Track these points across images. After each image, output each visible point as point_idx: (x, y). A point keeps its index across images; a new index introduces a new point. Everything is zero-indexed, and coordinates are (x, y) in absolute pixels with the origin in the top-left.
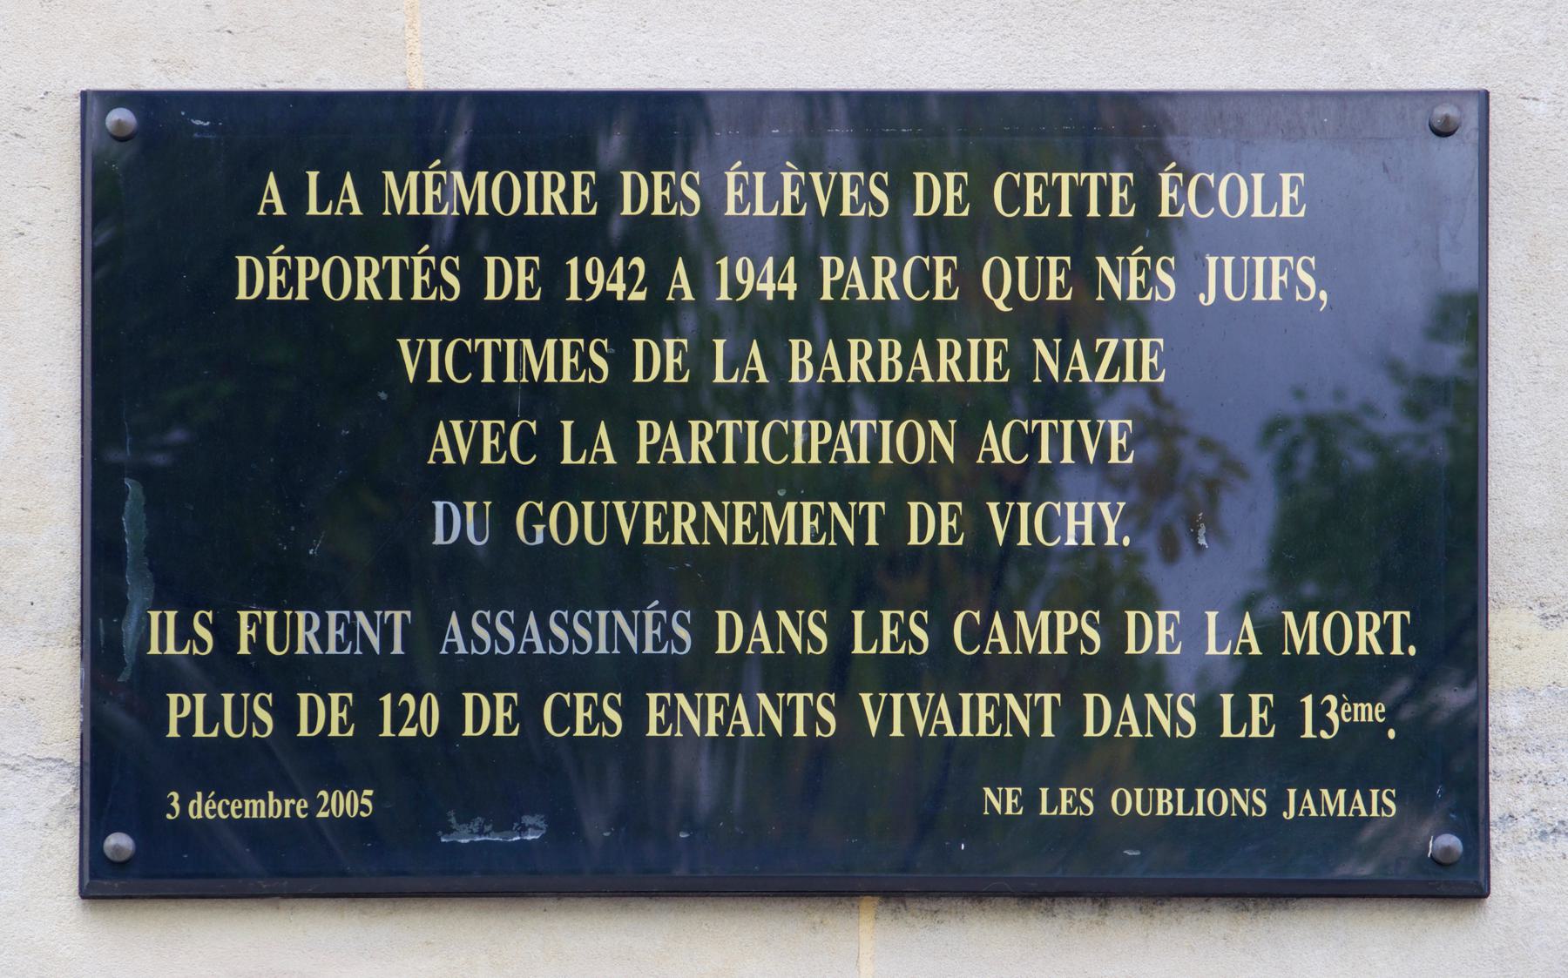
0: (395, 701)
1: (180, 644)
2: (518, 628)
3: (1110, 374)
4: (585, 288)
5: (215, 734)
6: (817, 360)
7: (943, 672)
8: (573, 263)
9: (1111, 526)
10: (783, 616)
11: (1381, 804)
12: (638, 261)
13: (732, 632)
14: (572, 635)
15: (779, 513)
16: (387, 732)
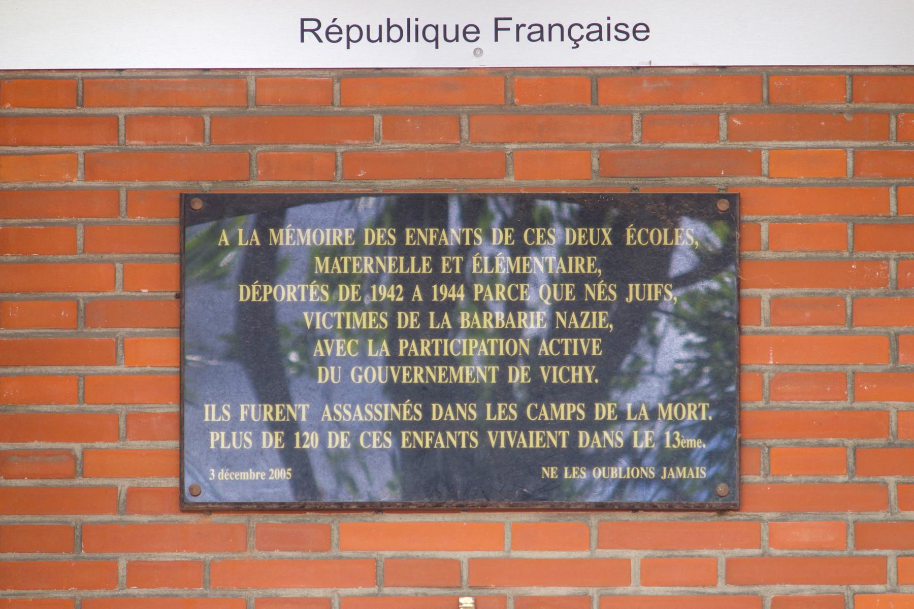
0: (301, 435)
1: (217, 417)
2: (353, 411)
3: (586, 325)
4: (440, 296)
5: (229, 447)
6: (471, 319)
7: (522, 425)
8: (435, 287)
9: (589, 375)
10: (458, 406)
11: (700, 473)
12: (400, 287)
13: (438, 412)
14: (374, 413)
15: (456, 370)
16: (298, 446)
